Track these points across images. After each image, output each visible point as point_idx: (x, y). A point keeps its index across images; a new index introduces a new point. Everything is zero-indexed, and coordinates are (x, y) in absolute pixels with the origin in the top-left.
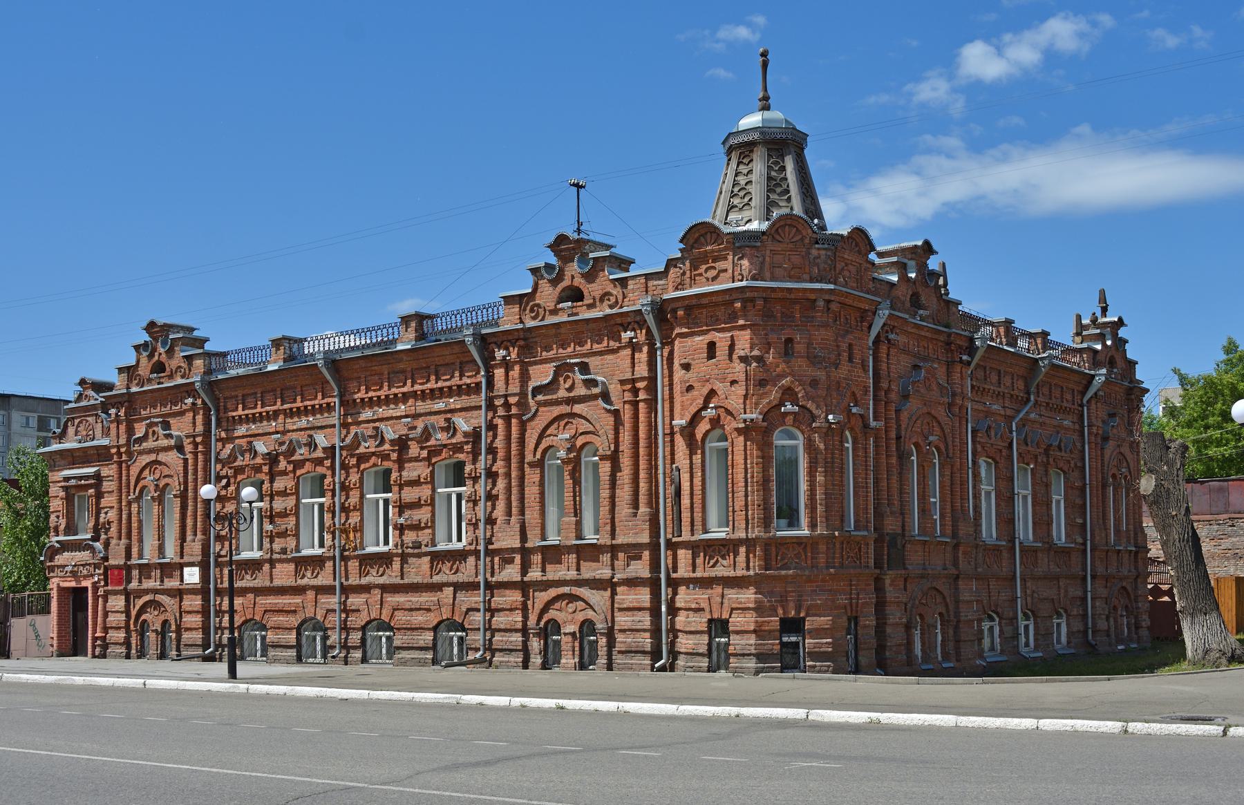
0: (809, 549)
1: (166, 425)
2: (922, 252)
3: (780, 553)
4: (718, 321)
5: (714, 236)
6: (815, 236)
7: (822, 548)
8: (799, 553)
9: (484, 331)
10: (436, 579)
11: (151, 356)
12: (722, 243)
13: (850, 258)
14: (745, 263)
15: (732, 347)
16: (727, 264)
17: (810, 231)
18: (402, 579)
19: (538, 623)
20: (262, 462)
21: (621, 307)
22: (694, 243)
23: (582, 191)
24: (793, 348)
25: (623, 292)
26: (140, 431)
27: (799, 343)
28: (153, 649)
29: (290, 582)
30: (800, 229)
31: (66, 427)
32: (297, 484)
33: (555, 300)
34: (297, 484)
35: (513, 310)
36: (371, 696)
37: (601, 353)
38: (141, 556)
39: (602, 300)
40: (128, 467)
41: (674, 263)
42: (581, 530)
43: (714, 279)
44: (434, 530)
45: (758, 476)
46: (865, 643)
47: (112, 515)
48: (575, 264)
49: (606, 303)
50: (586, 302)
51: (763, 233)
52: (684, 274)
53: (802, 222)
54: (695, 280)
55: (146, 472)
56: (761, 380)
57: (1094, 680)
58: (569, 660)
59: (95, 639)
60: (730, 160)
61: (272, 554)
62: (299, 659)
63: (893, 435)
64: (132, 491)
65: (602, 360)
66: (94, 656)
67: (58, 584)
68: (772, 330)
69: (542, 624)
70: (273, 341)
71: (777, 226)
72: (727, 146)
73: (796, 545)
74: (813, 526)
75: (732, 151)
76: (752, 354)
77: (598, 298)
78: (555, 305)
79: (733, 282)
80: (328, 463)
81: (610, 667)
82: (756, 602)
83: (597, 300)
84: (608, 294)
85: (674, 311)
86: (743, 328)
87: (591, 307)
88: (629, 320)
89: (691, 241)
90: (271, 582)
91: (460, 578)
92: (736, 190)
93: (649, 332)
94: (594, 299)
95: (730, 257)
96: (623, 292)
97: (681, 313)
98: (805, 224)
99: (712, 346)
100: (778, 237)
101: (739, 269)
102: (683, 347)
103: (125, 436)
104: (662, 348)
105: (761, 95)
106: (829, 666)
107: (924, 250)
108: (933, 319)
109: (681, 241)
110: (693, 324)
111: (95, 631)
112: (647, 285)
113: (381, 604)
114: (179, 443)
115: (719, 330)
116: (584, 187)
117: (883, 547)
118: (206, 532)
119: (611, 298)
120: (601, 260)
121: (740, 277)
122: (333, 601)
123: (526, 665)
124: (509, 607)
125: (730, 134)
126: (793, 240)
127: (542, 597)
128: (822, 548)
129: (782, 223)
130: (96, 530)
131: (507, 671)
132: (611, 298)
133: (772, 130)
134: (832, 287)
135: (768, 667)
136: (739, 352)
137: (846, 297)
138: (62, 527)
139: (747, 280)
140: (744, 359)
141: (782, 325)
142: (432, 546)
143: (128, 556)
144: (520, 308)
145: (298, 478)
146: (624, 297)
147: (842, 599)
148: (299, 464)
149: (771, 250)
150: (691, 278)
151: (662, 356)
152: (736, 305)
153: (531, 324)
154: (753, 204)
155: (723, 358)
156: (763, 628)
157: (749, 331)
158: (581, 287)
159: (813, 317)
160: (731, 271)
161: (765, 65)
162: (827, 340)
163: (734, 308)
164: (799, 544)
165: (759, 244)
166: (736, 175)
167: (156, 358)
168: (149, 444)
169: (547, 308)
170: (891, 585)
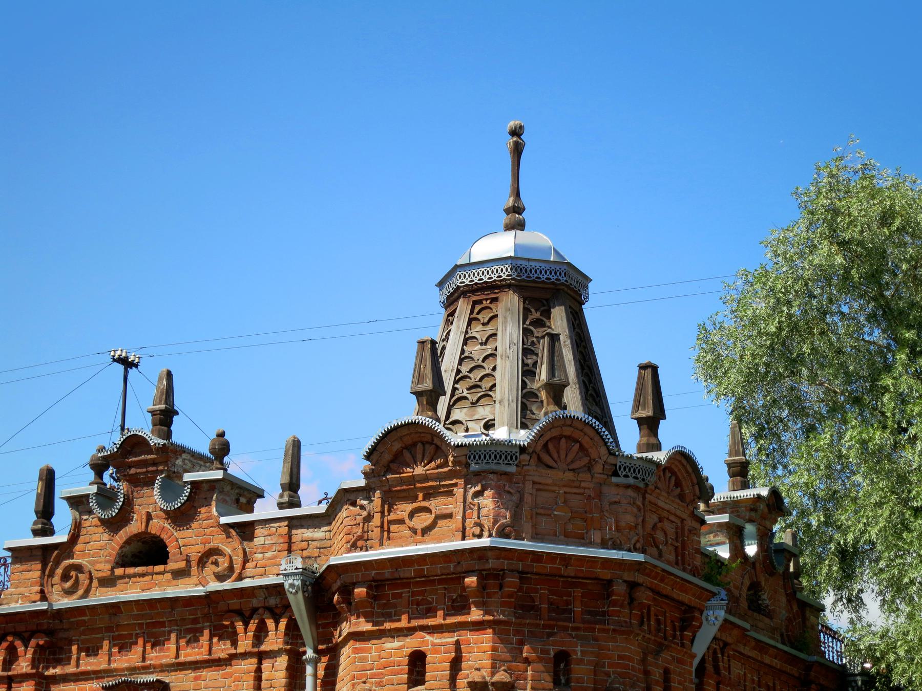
2: (766, 510)
4: (430, 612)
5: (430, 449)
6: (611, 460)
12: (445, 464)
13: (667, 507)
14: (487, 502)
15: (456, 665)
16: (452, 505)
17: (603, 450)
21: (240, 578)
22: (392, 461)
23: (132, 372)
24: (568, 672)
25: (244, 551)
27: (580, 662)
30: (586, 445)
33: (112, 558)
35: (29, 575)
37: (195, 665)
39: (202, 562)
41: (352, 497)
43: (426, 531)
48: (156, 491)
49: (210, 569)
50: (172, 565)
51: (523, 449)
52: (368, 518)
53: (591, 433)
54: (389, 531)
60: (452, 314)
65: (196, 679)
68: (532, 634)
71: (547, 437)
72: (449, 288)
75: (459, 298)
76: (495, 679)
77: (194, 557)
78: (112, 570)
79: (463, 539)
83: (194, 564)
84: (215, 551)
85: (347, 591)
86: (478, 626)
87: (179, 574)
88: (255, 603)
89: (387, 457)
92: (465, 369)
93: (293, 630)
94: (188, 561)
95: (459, 492)
96: (244, 551)
97: (360, 591)
98: (597, 438)
99: (417, 661)
100: (546, 458)
101: (475, 515)
102: (362, 660)
104: (315, 662)
105: (510, 202)
107: (768, 505)
108: (782, 635)
109: (368, 456)
110: (383, 615)
112: (290, 538)
115: (433, 630)
116: (136, 366)
119: (220, 559)
120: (205, 487)
121: (477, 530)
125: (457, 267)
126: (570, 467)
129: (555, 433)
132: (220, 559)
133: (533, 264)
134: (639, 557)
137: (662, 580)
139: (490, 536)
141: (552, 627)
144: (43, 570)
146: (246, 560)
149: (534, 483)
150: (382, 527)
151: (315, 676)
152: (357, 590)
153: (63, 602)
154: (497, 394)
155: (438, 683)
157: (488, 635)
158: (164, 536)
159: (604, 614)
160: (460, 517)
161: (518, 151)
163: (464, 588)
165: (512, 469)
166: (465, 342)
169: (96, 574)
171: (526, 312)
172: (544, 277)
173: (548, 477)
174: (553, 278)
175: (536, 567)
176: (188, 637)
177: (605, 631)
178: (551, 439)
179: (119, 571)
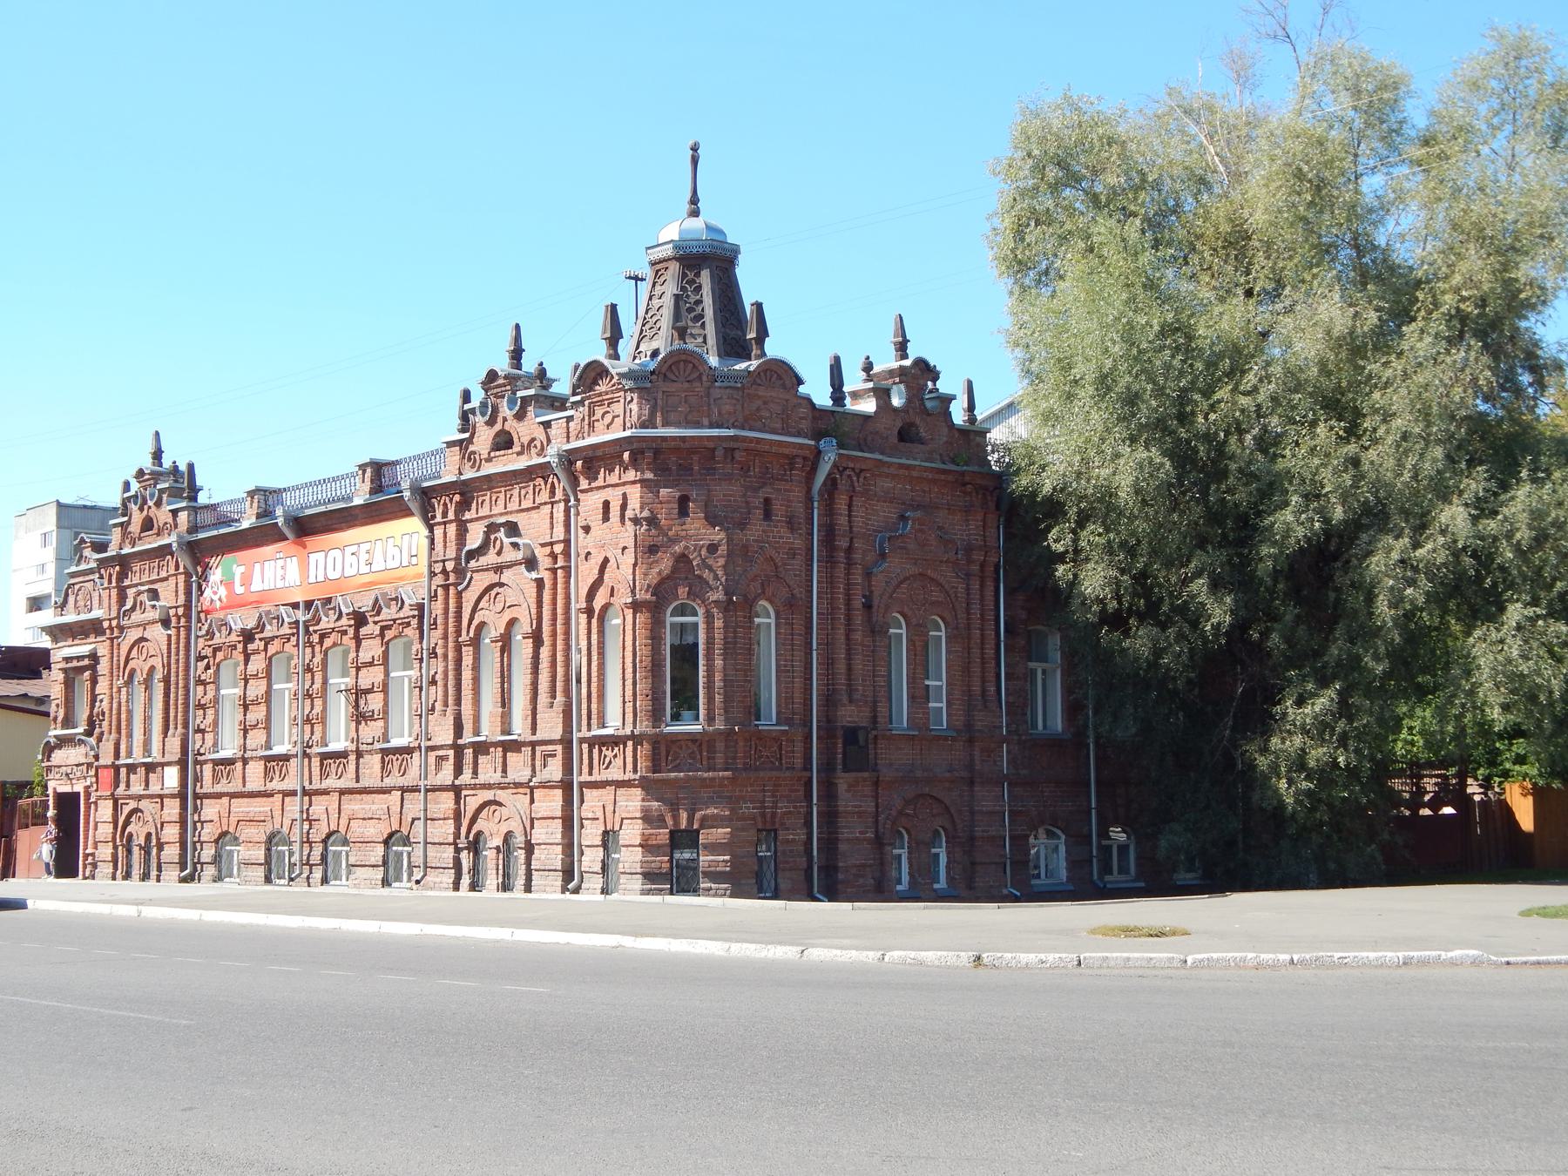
0: (704, 747)
1: (154, 595)
3: (672, 753)
7: (720, 746)
8: (693, 752)
9: (425, 484)
10: (388, 782)
11: (491, 422)
15: (624, 507)
18: (358, 781)
19: (467, 837)
20: (290, 631)
26: (474, 539)
28: (136, 872)
29: (377, 784)
31: (67, 595)
32: (269, 666)
34: (269, 666)
36: (382, 930)
38: (477, 733)
40: (459, 595)
42: (510, 723)
44: (386, 722)
45: (647, 661)
46: (787, 862)
47: (105, 705)
55: (134, 653)
56: (650, 546)
57: (949, 908)
58: (492, 880)
59: (86, 856)
61: (245, 752)
62: (268, 880)
63: (858, 602)
64: (121, 674)
65: (529, 518)
66: (85, 878)
67: (55, 789)
69: (471, 839)
70: (248, 492)
71: (669, 363)
73: (690, 743)
74: (710, 719)
78: (489, 453)
80: (294, 639)
81: (528, 888)
82: (642, 811)
89: (589, 381)
90: (244, 786)
91: (407, 781)
99: (606, 505)
103: (454, 548)
106: (726, 889)
111: (85, 849)
113: (339, 813)
114: (529, 553)
117: (836, 744)
118: (186, 725)
122: (294, 806)
123: (456, 887)
124: (442, 816)
127: (472, 803)
128: (720, 746)
129: (674, 359)
130: (91, 723)
131: (246, 884)
135: (655, 889)
136: (629, 514)
138: (60, 719)
140: (636, 521)
141: (676, 480)
142: (383, 742)
143: (117, 755)
145: (270, 658)
147: (748, 808)
148: (268, 642)
150: (589, 424)
156: (650, 842)
161: (695, 161)
162: (731, 496)
164: (694, 741)
165: (649, 385)
167: (145, 512)
168: (490, 558)
170: (848, 791)
171: (684, 275)
172: (695, 251)
173: (672, 387)
174: (701, 250)
175: (664, 445)
176: (649, 475)
177: (713, 480)
178: (673, 364)
179: (492, 454)
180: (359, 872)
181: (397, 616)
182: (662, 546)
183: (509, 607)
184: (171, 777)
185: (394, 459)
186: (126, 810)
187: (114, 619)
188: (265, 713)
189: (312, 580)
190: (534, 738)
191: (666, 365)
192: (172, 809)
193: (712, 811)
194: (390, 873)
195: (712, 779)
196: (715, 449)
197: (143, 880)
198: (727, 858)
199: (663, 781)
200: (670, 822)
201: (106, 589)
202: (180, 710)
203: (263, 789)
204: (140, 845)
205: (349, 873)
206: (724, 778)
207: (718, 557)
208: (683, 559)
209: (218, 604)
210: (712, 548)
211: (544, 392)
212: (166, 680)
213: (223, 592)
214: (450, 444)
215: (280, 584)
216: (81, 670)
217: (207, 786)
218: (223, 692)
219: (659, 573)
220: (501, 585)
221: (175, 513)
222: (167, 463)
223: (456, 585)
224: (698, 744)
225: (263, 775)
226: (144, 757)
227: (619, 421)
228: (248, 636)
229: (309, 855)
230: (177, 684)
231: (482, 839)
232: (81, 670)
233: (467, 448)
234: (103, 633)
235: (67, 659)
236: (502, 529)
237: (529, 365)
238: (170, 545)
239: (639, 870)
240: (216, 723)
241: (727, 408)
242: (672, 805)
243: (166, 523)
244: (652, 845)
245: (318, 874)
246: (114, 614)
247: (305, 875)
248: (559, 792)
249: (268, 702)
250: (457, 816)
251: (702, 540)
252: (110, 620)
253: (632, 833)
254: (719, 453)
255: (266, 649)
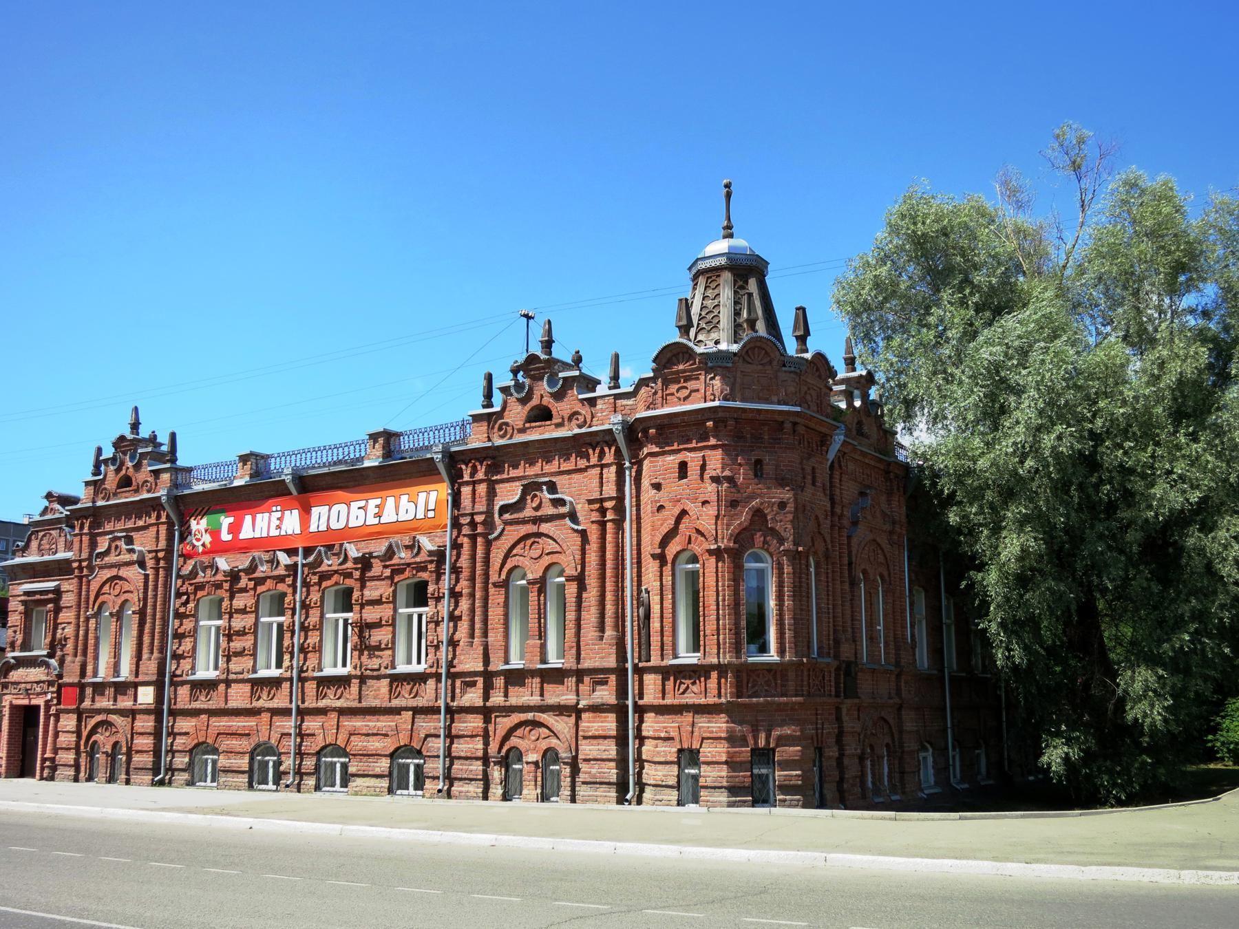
1: (129, 541)
3: (751, 680)
7: (791, 675)
9: (453, 449)
10: (396, 703)
15: (703, 468)
18: (360, 702)
32: (257, 602)
34: (257, 602)
44: (394, 652)
46: (830, 776)
47: (69, 631)
55: (106, 589)
61: (228, 675)
66: (42, 778)
67: (11, 702)
74: (781, 651)
78: (524, 425)
80: (289, 581)
90: (226, 704)
106: (798, 800)
113: (338, 729)
118: (162, 649)
122: (289, 724)
124: (470, 733)
135: (739, 801)
136: (710, 472)
138: (19, 642)
140: (716, 480)
142: (318, 671)
143: (83, 673)
150: (663, 397)
165: (730, 365)
172: (744, 263)
174: (749, 263)
180: (359, 781)
181: (413, 560)
182: (741, 501)
183: (548, 554)
184: (146, 695)
185: (399, 431)
186: (92, 722)
187: (84, 560)
188: (252, 642)
189: (313, 528)
190: (137, 680)
191: (745, 350)
192: (146, 723)
193: (787, 731)
194: (396, 781)
195: (786, 704)
196: (783, 422)
197: (109, 782)
198: (799, 772)
199: (745, 705)
200: (751, 742)
201: (76, 535)
202: (156, 637)
203: (249, 706)
204: (106, 753)
205: (345, 784)
206: (795, 703)
207: (787, 513)
208: (758, 514)
209: (201, 549)
210: (782, 505)
211: (156, 450)
212: (142, 613)
213: (207, 539)
214: (477, 418)
215: (274, 533)
216: (44, 602)
217: (650, 697)
218: (202, 623)
219: (739, 525)
220: (121, 578)
221: (156, 473)
222: (144, 433)
223: (87, 576)
224: (772, 673)
225: (249, 694)
226: (114, 677)
227: (700, 395)
228: (234, 576)
229: (171, 761)
230: (154, 615)
231: (118, 746)
232: (44, 602)
233: (100, 486)
234: (71, 571)
235: (27, 593)
236: (544, 487)
237: (144, 433)
238: (159, 498)
239: (725, 784)
240: (194, 649)
241: (792, 389)
242: (752, 726)
243: (147, 481)
244: (736, 762)
245: (311, 782)
246: (85, 555)
247: (296, 782)
248: (152, 717)
249: (255, 633)
250: (78, 733)
251: (774, 498)
252: (80, 561)
253: (714, 751)
254: (788, 426)
255: (255, 589)
